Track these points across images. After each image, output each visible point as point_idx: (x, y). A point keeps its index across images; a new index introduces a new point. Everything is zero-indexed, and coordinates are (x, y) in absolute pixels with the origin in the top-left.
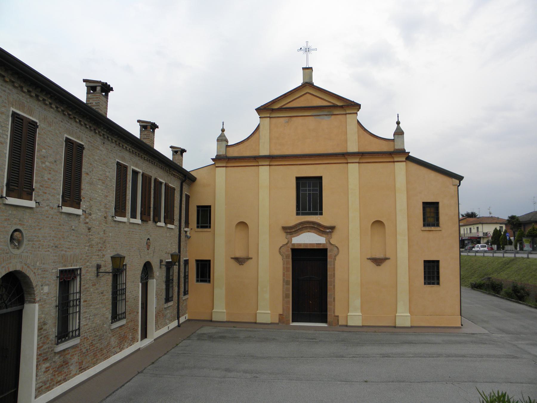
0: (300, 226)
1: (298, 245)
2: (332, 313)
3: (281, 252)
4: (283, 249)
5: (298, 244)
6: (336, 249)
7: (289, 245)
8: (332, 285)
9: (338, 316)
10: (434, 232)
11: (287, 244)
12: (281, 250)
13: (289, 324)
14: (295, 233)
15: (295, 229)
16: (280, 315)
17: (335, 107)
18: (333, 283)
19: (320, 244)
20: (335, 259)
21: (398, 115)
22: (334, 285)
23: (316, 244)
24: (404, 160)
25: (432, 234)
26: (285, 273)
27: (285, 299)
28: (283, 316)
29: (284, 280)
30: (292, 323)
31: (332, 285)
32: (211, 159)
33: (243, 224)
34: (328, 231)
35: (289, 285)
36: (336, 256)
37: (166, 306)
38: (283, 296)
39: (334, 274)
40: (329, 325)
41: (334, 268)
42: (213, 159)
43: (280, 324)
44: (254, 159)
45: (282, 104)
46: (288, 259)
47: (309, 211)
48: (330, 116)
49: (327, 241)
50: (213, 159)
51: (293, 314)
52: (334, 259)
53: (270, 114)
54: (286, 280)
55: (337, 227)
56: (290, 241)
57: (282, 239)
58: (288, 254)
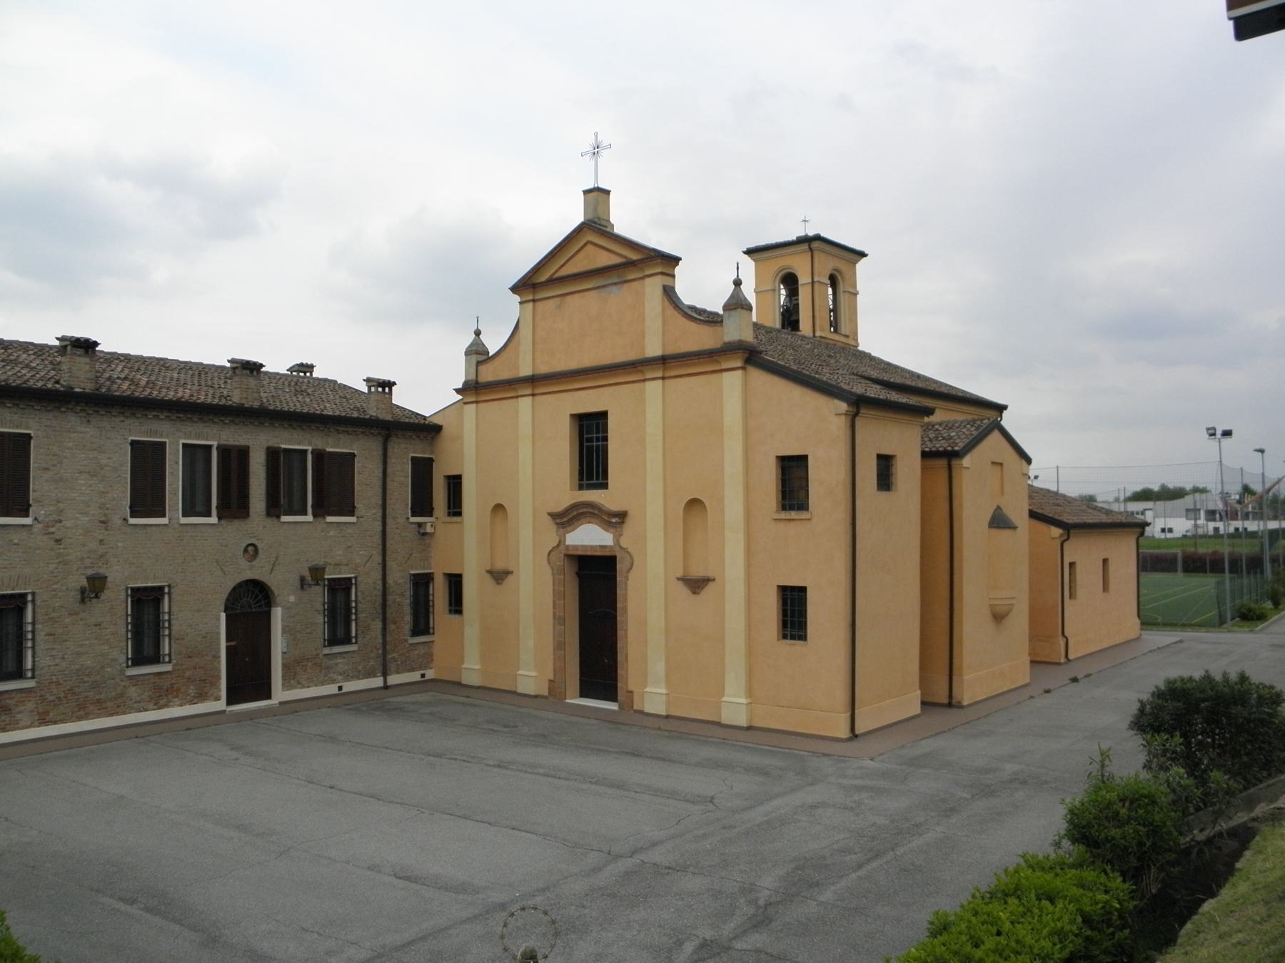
0: (573, 512)
7: (562, 547)
9: (631, 692)
10: (797, 522)
11: (558, 545)
16: (550, 681)
17: (629, 264)
21: (478, 318)
24: (739, 363)
25: (795, 530)
29: (554, 613)
32: (454, 389)
33: (499, 508)
34: (614, 520)
37: (327, 651)
42: (458, 391)
44: (709, 357)
45: (552, 272)
47: (603, 480)
48: (620, 286)
50: (458, 391)
53: (534, 293)
55: (630, 513)
57: (551, 538)
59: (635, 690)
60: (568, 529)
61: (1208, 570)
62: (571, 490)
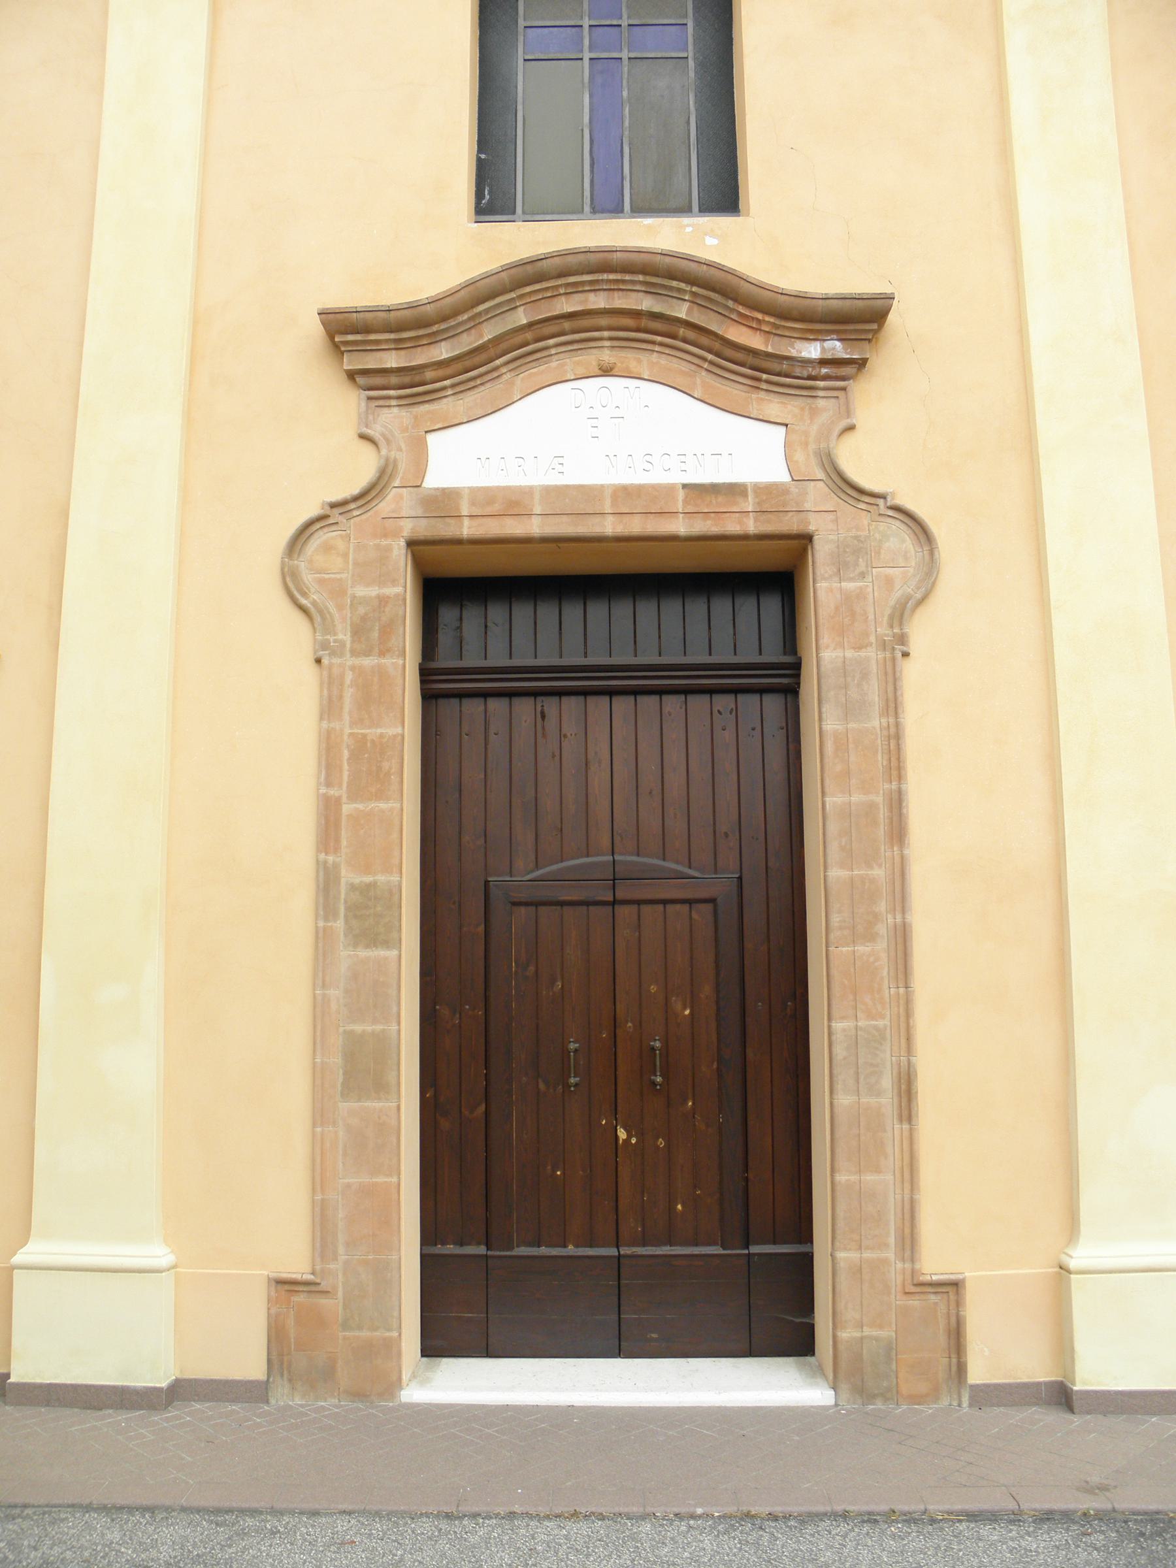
1: (496, 508)
2: (890, 1255)
3: (308, 578)
4: (327, 548)
5: (485, 496)
6: (898, 537)
8: (871, 937)
11: (366, 496)
12: (302, 565)
13: (398, 1384)
14: (461, 389)
15: (467, 342)
16: (285, 1285)
18: (882, 907)
19: (734, 490)
20: (902, 639)
22: (902, 937)
23: (691, 488)
26: (347, 808)
27: (344, 1106)
28: (323, 1301)
29: (327, 881)
30: (424, 1382)
31: (882, 929)
34: (812, 351)
35: (386, 944)
36: (901, 613)
38: (318, 1073)
39: (897, 802)
40: (863, 1392)
41: (895, 738)
43: (282, 1396)
46: (382, 654)
49: (799, 456)
51: (429, 1264)
52: (883, 645)
54: (352, 887)
56: (402, 467)
58: (383, 601)
59: (970, 1275)
60: (448, 405)
61: (537, 497)
62: (739, 216)
